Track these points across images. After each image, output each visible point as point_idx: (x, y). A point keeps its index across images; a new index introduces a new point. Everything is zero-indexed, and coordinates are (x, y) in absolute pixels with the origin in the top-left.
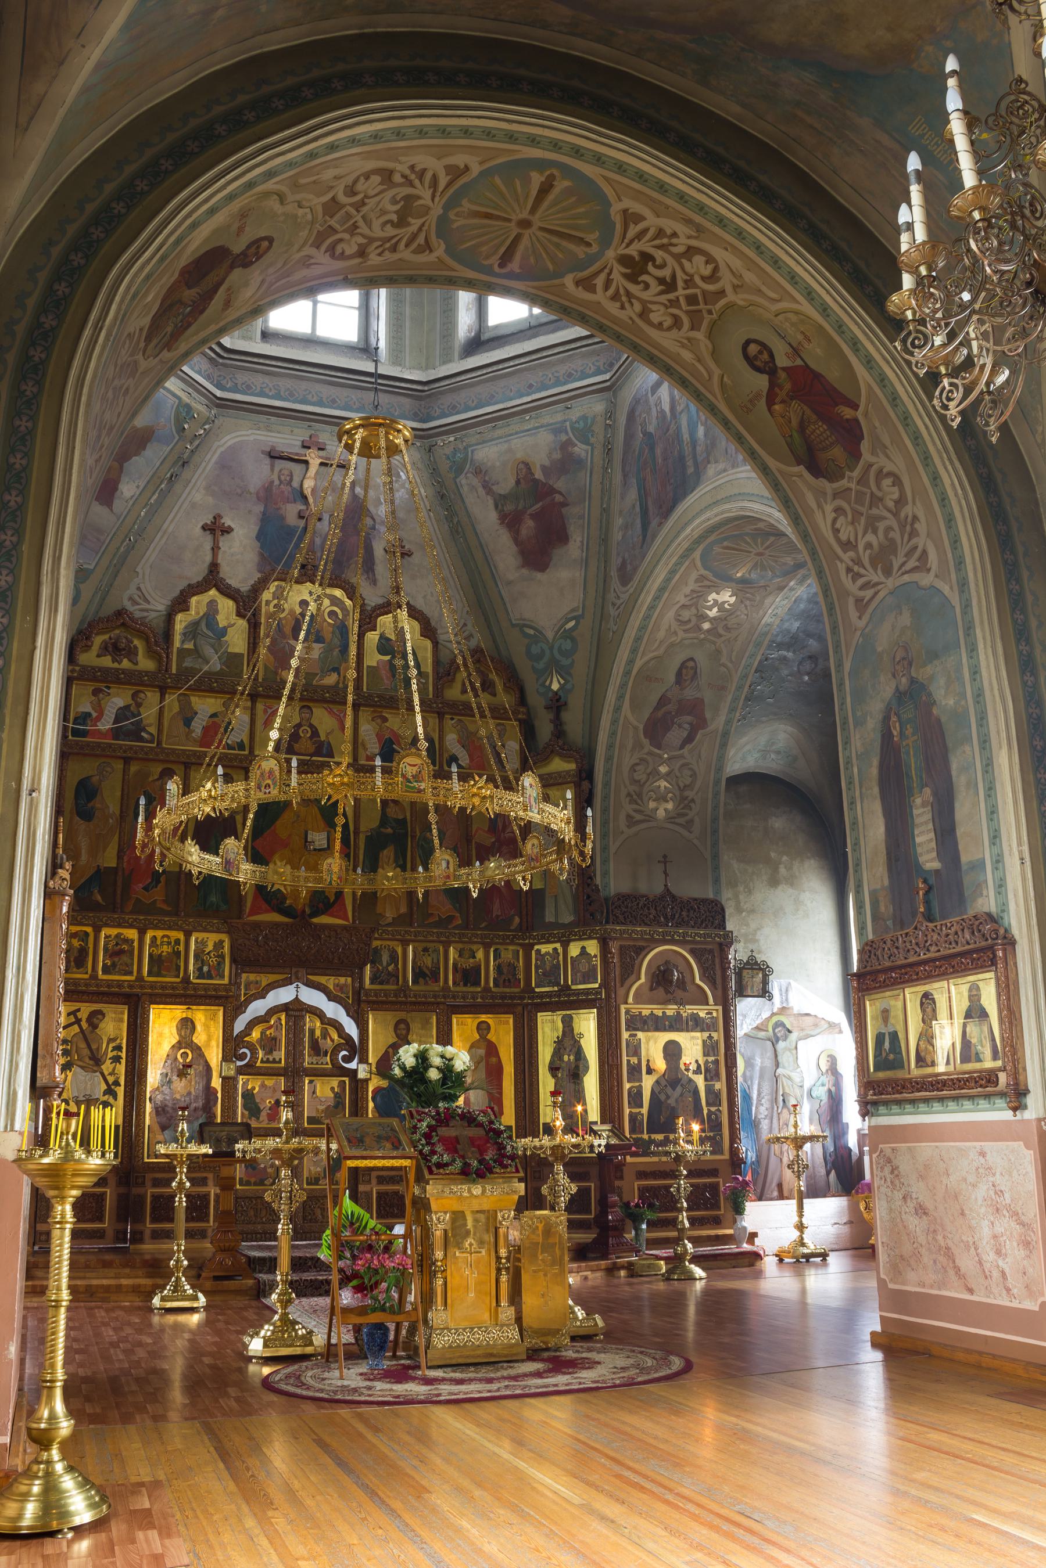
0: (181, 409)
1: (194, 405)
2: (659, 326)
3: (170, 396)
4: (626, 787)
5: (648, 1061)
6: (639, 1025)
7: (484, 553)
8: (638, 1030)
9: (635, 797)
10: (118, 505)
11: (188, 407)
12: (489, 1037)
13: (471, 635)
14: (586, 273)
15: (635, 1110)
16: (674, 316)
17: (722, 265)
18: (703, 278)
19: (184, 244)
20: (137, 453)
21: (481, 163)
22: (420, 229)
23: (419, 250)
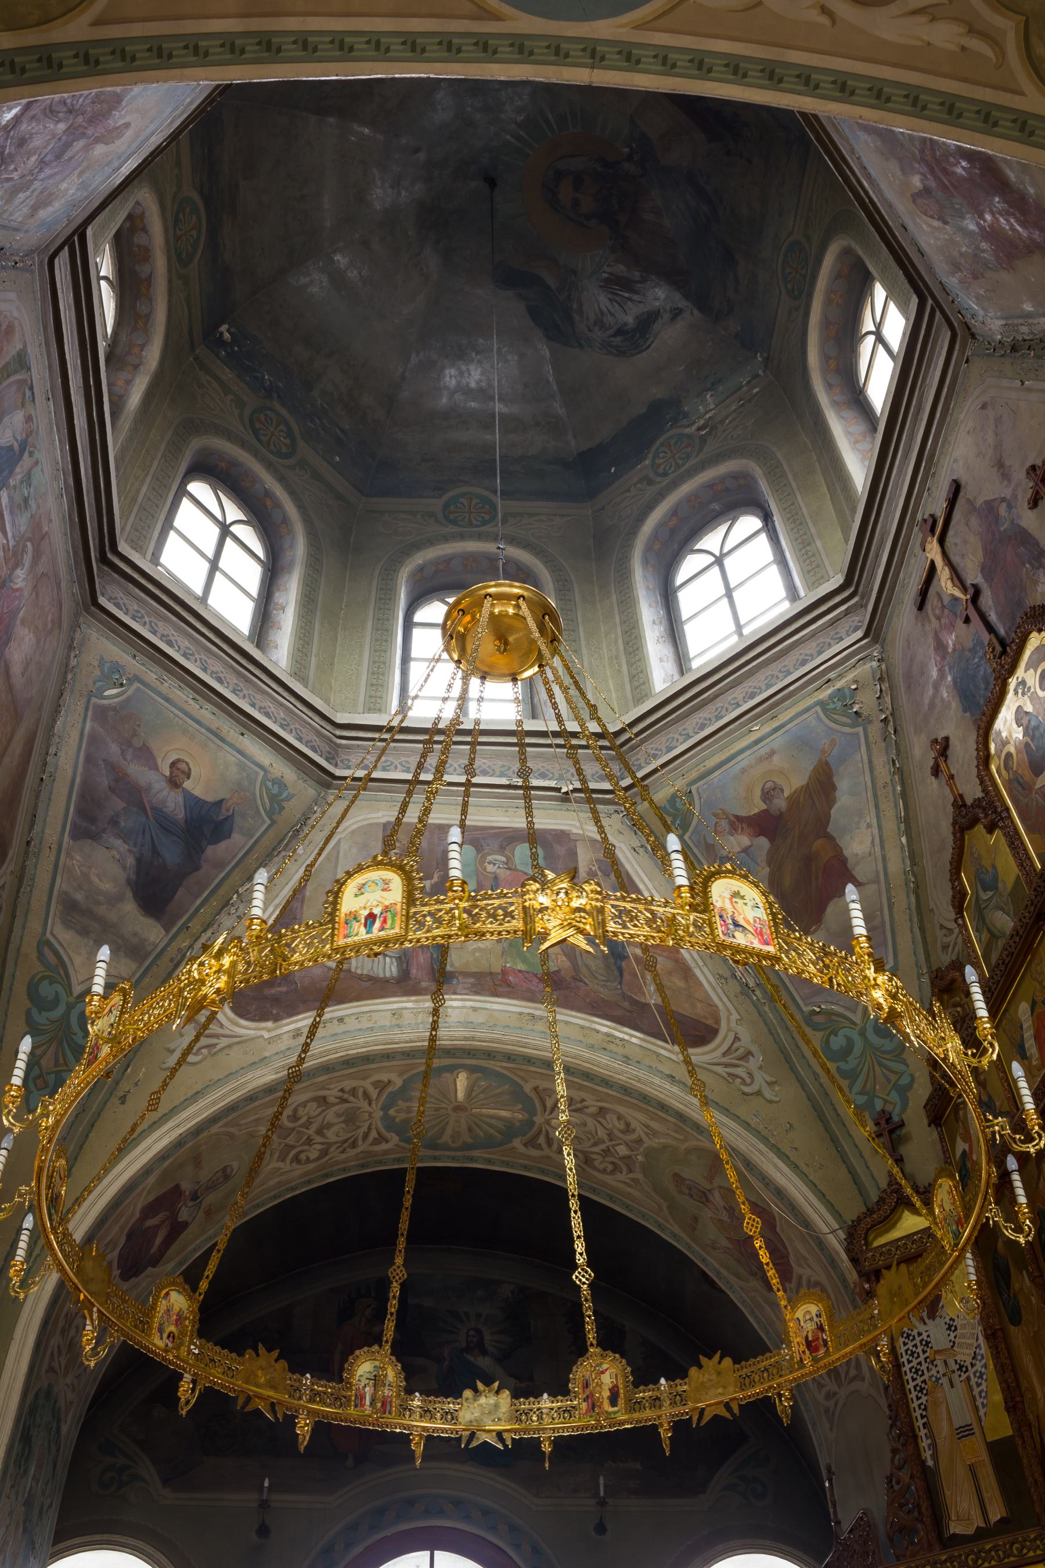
0: (832, 706)
1: (839, 685)
2: (604, 1171)
3: (805, 716)
7: (922, 929)
13: (749, 1053)
14: (530, 1135)
16: (612, 1163)
17: (629, 1118)
18: (623, 1132)
19: (121, 1208)
20: (831, 801)
21: (400, 1075)
22: (369, 1129)
23: (376, 1142)
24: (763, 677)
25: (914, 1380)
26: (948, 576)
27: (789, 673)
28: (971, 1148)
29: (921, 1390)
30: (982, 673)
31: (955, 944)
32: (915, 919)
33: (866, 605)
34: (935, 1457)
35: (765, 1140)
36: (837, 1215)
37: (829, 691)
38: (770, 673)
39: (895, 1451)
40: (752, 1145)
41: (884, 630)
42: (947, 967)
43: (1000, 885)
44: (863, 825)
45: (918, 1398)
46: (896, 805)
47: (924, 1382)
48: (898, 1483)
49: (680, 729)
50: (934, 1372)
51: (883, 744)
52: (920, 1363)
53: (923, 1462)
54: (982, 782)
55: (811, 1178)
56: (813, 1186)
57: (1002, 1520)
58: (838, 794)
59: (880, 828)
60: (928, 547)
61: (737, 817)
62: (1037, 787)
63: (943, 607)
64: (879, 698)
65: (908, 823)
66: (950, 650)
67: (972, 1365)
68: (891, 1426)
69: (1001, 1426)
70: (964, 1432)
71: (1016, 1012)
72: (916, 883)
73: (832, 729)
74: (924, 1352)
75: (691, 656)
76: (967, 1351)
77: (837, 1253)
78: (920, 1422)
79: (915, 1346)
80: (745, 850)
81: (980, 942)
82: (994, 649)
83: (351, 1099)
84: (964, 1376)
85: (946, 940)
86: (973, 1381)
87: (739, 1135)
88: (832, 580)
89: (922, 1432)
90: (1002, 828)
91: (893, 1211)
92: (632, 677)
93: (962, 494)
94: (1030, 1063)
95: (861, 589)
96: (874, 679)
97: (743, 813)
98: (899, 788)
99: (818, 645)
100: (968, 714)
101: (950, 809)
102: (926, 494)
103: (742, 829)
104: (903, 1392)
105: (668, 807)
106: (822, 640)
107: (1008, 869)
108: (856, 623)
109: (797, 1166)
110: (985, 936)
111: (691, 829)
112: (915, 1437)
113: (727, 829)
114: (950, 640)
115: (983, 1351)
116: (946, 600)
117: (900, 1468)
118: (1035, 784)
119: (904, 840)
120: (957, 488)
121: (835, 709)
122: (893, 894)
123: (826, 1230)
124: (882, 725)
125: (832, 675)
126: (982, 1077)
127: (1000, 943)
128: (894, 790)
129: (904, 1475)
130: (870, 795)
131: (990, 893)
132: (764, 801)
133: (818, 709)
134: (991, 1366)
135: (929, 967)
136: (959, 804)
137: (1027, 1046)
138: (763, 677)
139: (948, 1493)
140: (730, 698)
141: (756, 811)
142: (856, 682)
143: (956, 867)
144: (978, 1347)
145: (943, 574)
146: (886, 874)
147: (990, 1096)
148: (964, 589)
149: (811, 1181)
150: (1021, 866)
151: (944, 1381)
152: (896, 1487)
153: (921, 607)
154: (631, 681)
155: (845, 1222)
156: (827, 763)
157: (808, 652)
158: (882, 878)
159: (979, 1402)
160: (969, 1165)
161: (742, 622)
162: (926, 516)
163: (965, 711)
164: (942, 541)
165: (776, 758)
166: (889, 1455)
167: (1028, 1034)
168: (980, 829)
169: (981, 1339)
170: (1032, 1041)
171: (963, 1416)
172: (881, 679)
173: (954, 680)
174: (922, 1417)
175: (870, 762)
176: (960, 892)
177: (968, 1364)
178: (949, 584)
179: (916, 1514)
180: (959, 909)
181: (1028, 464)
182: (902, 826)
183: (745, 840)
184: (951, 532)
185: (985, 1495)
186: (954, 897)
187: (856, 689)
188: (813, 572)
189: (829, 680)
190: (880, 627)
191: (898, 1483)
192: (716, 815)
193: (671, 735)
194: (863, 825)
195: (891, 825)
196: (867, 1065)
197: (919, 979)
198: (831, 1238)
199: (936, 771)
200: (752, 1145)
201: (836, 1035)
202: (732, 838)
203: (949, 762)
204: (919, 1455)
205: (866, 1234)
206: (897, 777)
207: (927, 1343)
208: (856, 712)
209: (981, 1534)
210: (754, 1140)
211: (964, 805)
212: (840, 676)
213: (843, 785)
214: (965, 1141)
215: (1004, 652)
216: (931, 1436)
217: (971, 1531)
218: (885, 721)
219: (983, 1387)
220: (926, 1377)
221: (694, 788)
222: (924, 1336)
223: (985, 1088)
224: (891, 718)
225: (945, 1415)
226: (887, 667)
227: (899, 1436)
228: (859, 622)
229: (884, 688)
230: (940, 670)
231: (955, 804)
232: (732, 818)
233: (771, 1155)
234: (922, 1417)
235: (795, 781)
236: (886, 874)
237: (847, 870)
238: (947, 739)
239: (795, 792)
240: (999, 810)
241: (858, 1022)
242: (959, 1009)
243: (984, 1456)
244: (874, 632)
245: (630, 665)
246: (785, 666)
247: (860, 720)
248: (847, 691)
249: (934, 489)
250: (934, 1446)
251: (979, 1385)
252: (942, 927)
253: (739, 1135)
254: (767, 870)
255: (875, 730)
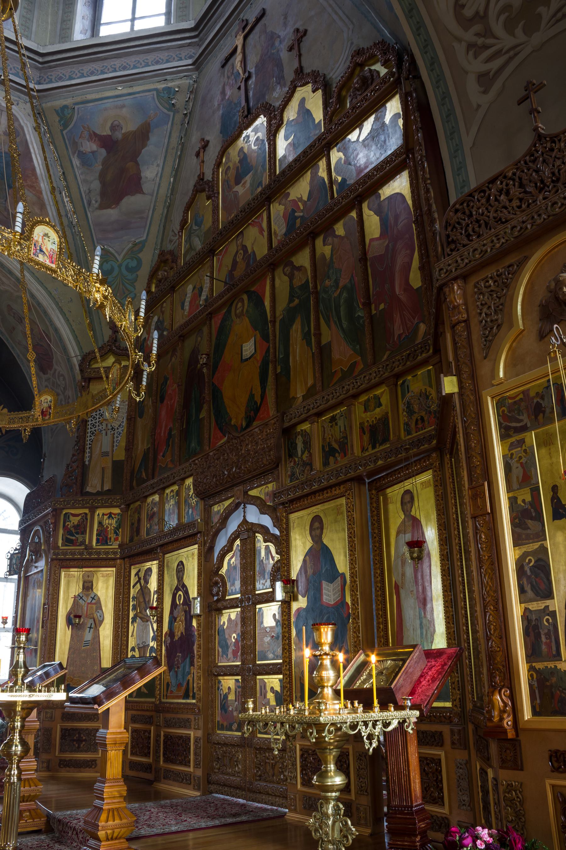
0: (162, 95)
1: (170, 85)
3: (147, 94)
4: (459, 40)
5: (555, 489)
6: (525, 419)
7: (164, 227)
8: (524, 429)
9: (480, 41)
10: (146, 187)
11: (168, 89)
12: (413, 513)
15: (535, 606)
20: (144, 145)
24: (133, 60)
25: (91, 428)
26: (240, 60)
27: (147, 65)
28: (148, 338)
29: (93, 434)
30: (235, 119)
31: (176, 242)
32: (163, 221)
33: (200, 46)
34: (90, 461)
35: (57, 304)
36: (80, 348)
37: (163, 86)
38: (138, 59)
39: (74, 455)
40: (50, 304)
41: (203, 66)
42: (167, 251)
43: (203, 226)
44: (155, 164)
45: (90, 436)
46: (175, 161)
47: (95, 430)
48: (71, 468)
49: (80, 68)
50: (100, 427)
51: (180, 127)
52: (96, 423)
53: (84, 462)
54: (213, 174)
55: (73, 327)
56: (73, 331)
57: (109, 490)
58: (149, 143)
59: (163, 169)
60: (238, 37)
61: (94, 133)
62: (234, 190)
63: (233, 73)
64: (187, 101)
65: (177, 172)
66: (227, 98)
67: (118, 429)
68: (75, 445)
69: (121, 455)
70: (105, 454)
71: (187, 287)
72: (169, 206)
73: (158, 107)
74: (99, 418)
75: (102, 22)
76: (118, 423)
77: (75, 365)
78: (88, 442)
79: (96, 415)
80: (93, 152)
81: (185, 247)
82: (244, 111)
83: (490, 41)
84: (113, 432)
85: (172, 238)
86: (116, 435)
87: (44, 297)
88: (189, 22)
89: (88, 450)
90: (213, 201)
91: (106, 354)
92: (63, 21)
93: (264, 19)
94: (184, 312)
95: (201, 35)
96: (188, 90)
97: (98, 132)
98: (179, 153)
99: (168, 56)
100: (221, 135)
101: (196, 178)
102: (249, 5)
103: (95, 140)
104: (85, 432)
105: (60, 111)
106: (171, 54)
107: (208, 223)
108: (191, 53)
109: (68, 320)
110: (188, 246)
111: (68, 129)
112: (84, 452)
113: (87, 137)
114: (228, 93)
115: (124, 424)
116: (235, 71)
117: (73, 462)
118: (234, 188)
119: (172, 179)
120: (263, 14)
121: (163, 97)
122: (157, 204)
123: (73, 355)
124: (184, 116)
125: (168, 77)
126: (163, 309)
127: (193, 253)
128: (177, 153)
129: (74, 465)
130: (164, 150)
131: (197, 228)
132: (111, 131)
133: (155, 93)
134: (125, 431)
135: (161, 247)
136: (201, 178)
137: (185, 304)
138: (133, 60)
139: (90, 476)
140: (112, 63)
141: (105, 134)
142: (179, 87)
143: (188, 207)
144: (123, 422)
145: (239, 57)
146: (157, 193)
147: (163, 318)
148: (245, 71)
149: (73, 329)
150: (213, 222)
151: (104, 432)
152: (70, 469)
153: (223, 66)
154: (61, 23)
155: (83, 352)
156: (149, 124)
157: (162, 57)
158: (155, 194)
159: (115, 444)
160: (145, 345)
161: (136, 16)
162: (244, 18)
163: (221, 133)
164: (245, 38)
165: (124, 110)
166: (71, 456)
167: (188, 300)
168: (204, 195)
169: (125, 419)
170: (188, 303)
171: (106, 447)
172: (191, 92)
173: (223, 114)
174: (90, 444)
175: (170, 133)
176: (185, 220)
177: (116, 428)
178: (239, 65)
179: (75, 481)
180: (182, 228)
181: (296, 26)
182: (174, 172)
183: (94, 147)
184: (251, 36)
185: (105, 480)
186: (182, 221)
187: (177, 91)
188: (181, 18)
189: (166, 80)
190: (201, 63)
191: (71, 468)
192: (84, 127)
193: (74, 70)
194: (155, 164)
195: (168, 170)
196: (116, 283)
197: (154, 250)
198: (75, 359)
199: (198, 155)
200: (50, 304)
201: (107, 263)
202: (88, 143)
203: (205, 153)
204: (83, 459)
205: (90, 361)
206: (180, 147)
207: (102, 415)
208: (173, 104)
209: (98, 493)
210: (51, 302)
211: (203, 179)
212: (172, 80)
213: (153, 139)
214: (147, 334)
215: (247, 116)
216: (91, 453)
217: (95, 491)
218: (185, 115)
219: (119, 439)
220: (96, 429)
221: (76, 107)
222: (102, 412)
223: (163, 314)
224: (188, 115)
225: (99, 446)
226: (197, 87)
227: (78, 450)
228: (194, 53)
229: (191, 97)
230: (219, 105)
231: (199, 176)
232: (92, 132)
233: (57, 311)
234: (90, 444)
235: (130, 126)
236: (157, 193)
237: (140, 183)
238: (208, 142)
239: (128, 132)
240: (215, 191)
241: (120, 260)
242: (166, 273)
243: (110, 465)
244: (198, 64)
245: (64, 12)
246: (147, 59)
247: (173, 109)
248: (172, 90)
249: (253, 5)
250: (91, 457)
251: (117, 437)
252: (173, 231)
253: (44, 297)
254: (101, 167)
255: (179, 117)
